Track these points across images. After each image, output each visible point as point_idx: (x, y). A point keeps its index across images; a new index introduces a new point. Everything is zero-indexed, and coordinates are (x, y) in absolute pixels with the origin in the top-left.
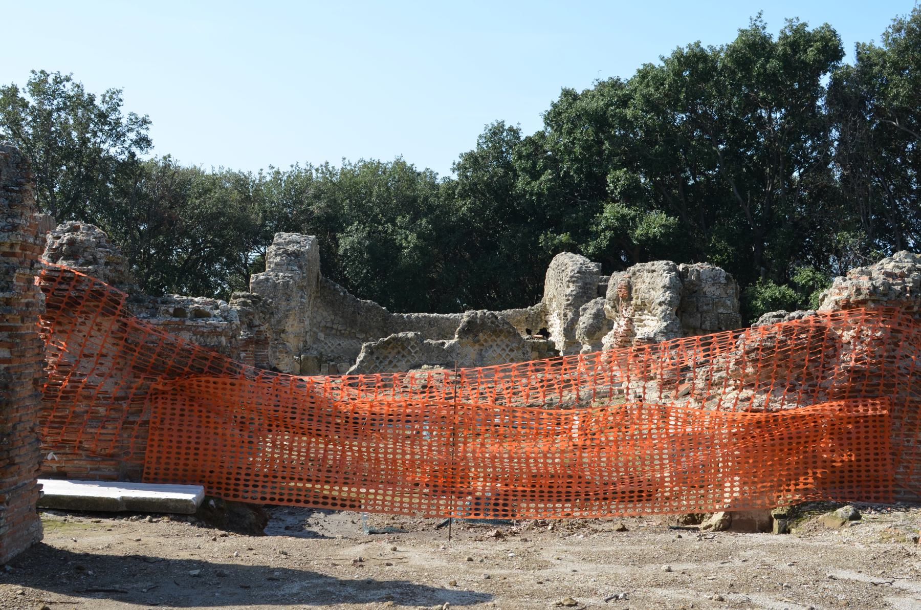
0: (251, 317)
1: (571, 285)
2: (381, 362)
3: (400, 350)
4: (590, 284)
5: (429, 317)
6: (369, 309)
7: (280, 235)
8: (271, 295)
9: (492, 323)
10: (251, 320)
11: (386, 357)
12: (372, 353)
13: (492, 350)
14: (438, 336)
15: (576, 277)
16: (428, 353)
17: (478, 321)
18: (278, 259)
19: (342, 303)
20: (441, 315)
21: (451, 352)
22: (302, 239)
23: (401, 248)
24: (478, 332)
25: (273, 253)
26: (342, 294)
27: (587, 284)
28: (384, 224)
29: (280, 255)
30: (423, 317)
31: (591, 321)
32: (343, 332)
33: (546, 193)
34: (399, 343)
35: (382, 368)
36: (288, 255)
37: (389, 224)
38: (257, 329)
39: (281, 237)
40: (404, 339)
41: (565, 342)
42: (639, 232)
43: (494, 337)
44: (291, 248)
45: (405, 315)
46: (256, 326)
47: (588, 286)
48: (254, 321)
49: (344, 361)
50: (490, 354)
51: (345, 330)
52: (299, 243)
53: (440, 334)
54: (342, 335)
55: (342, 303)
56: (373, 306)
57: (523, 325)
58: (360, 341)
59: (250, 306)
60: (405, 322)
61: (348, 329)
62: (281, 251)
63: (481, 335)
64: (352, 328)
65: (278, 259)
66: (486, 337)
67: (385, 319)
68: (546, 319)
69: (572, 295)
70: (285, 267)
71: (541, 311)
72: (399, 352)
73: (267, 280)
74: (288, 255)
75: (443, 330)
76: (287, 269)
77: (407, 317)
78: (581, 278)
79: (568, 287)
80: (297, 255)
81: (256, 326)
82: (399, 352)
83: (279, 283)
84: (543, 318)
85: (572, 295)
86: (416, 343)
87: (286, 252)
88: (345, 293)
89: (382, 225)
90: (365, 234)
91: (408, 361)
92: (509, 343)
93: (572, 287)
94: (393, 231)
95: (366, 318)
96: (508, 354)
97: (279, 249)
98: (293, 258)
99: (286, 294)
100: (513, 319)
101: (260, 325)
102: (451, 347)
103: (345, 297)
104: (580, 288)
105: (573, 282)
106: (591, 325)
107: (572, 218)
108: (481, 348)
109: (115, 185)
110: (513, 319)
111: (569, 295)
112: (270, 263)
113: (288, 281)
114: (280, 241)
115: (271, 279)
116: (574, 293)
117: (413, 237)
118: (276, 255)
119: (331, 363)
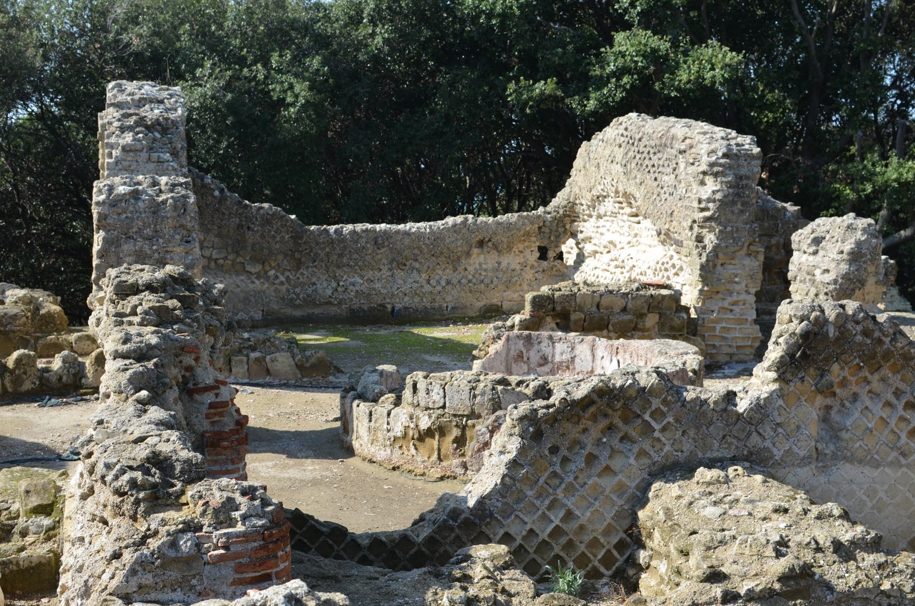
0: (189, 360)
1: (709, 180)
2: (565, 460)
3: (617, 421)
4: (748, 178)
5: (375, 231)
6: (267, 220)
7: (120, 85)
8: (148, 232)
9: (866, 333)
10: (189, 369)
11: (577, 443)
12: (538, 436)
13: (859, 406)
14: (391, 263)
15: (720, 165)
16: (698, 428)
17: (832, 332)
18: (128, 138)
19: (217, 210)
20: (394, 227)
21: (761, 421)
22: (165, 94)
23: (282, 102)
24: (827, 360)
25: (116, 124)
26: (217, 193)
27: (741, 178)
28: (251, 65)
29: (130, 128)
30: (363, 231)
31: (844, 267)
32: (221, 261)
33: (517, 13)
34: (619, 405)
35: (571, 479)
36: (148, 128)
37: (259, 66)
38: (209, 398)
39: (122, 91)
40: (633, 393)
41: (701, 291)
42: (683, 76)
43: (865, 373)
44: (152, 113)
45: (332, 228)
46: (208, 389)
47: (744, 182)
48: (199, 371)
49: (278, 350)
50: (854, 419)
51: (225, 258)
52: (161, 102)
53: (393, 260)
54: (220, 267)
55: (217, 210)
56: (274, 214)
57: (533, 239)
58: (253, 278)
59: (178, 320)
60: (332, 242)
61: (231, 257)
62: (131, 121)
63: (835, 368)
64: (238, 254)
65: (128, 138)
66: (846, 373)
67: (297, 236)
68: (574, 228)
69: (714, 201)
70: (144, 155)
71: (565, 215)
72: (610, 428)
73: (136, 195)
74: (148, 128)
75: (399, 253)
76: (149, 159)
77: (336, 231)
78: (730, 167)
79: (702, 183)
80: (162, 127)
81: (208, 389)
82: (610, 428)
83: (164, 202)
84: (568, 227)
85: (714, 201)
86: (665, 402)
87: (141, 121)
88: (222, 191)
89: (249, 66)
90: (222, 83)
91: (642, 453)
92: (902, 386)
93: (712, 186)
94: (266, 78)
95: (263, 237)
96: (902, 419)
97: (127, 116)
98: (157, 135)
99: (182, 226)
100: (519, 230)
101: (218, 384)
102: (760, 408)
103: (222, 199)
104: (730, 185)
105: (716, 175)
106: (846, 277)
107: (556, 54)
108: (829, 401)
109: (225, 407)
110: (519, 230)
111: (709, 200)
112: (112, 146)
113: (185, 197)
114: (121, 98)
115: (144, 192)
116: (718, 196)
117: (301, 88)
118: (123, 129)
119: (254, 355)
